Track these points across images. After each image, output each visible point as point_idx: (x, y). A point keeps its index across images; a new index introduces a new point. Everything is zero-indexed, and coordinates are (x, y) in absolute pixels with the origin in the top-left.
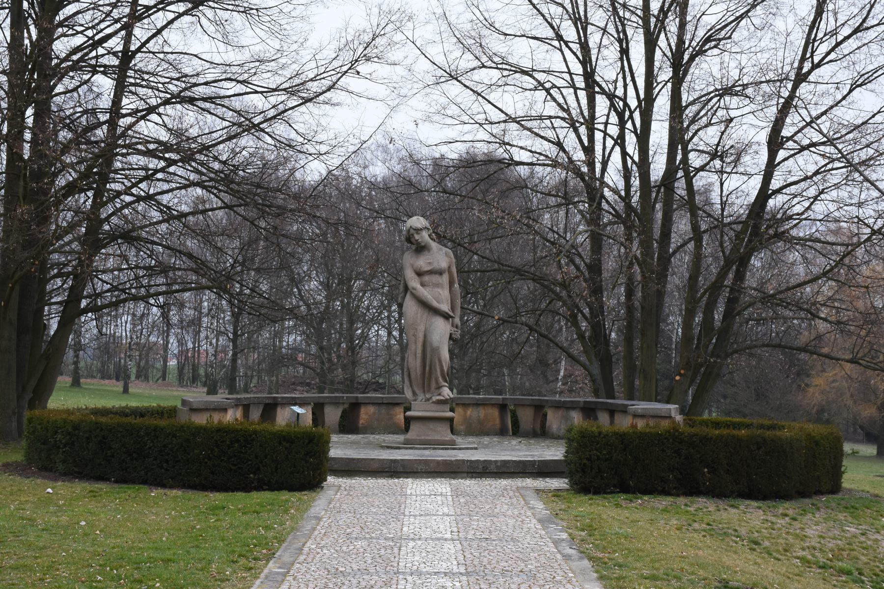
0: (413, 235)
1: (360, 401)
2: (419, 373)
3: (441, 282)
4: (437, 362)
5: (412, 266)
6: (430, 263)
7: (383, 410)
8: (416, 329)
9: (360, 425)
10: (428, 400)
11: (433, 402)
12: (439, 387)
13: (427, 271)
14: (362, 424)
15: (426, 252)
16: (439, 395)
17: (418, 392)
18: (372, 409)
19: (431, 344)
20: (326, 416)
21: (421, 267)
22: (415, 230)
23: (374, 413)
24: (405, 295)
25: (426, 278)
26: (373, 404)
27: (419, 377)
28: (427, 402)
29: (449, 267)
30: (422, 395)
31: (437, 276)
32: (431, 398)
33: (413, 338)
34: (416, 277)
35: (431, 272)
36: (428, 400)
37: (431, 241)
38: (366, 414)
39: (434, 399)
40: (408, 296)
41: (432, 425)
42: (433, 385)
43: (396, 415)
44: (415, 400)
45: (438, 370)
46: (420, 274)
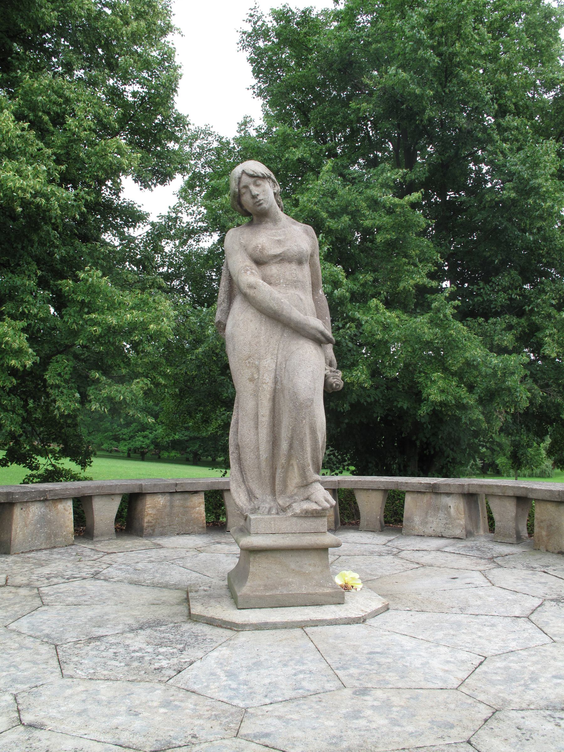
0: (246, 187)
1: (144, 492)
2: (264, 453)
3: (300, 277)
4: (307, 431)
5: (245, 248)
6: (279, 241)
7: (178, 500)
8: (258, 369)
9: (145, 525)
10: (284, 510)
11: (295, 516)
12: (306, 485)
13: (275, 256)
14: (148, 522)
15: (270, 225)
16: (308, 499)
17: (258, 492)
18: (161, 500)
19: (295, 396)
20: (96, 513)
21: (263, 248)
22: (252, 176)
23: (165, 506)
24: (229, 308)
25: (274, 269)
26: (163, 493)
27: (263, 464)
28: (282, 515)
29: (312, 256)
30: (269, 498)
31: (294, 266)
32: (290, 506)
33: (250, 386)
34: (254, 266)
35: (282, 259)
36: (284, 510)
37: (279, 209)
38: (154, 507)
39: (300, 507)
40: (238, 305)
41: (292, 562)
42: (295, 479)
43: (194, 508)
44: (255, 510)
45: (309, 449)
46: (259, 262)
